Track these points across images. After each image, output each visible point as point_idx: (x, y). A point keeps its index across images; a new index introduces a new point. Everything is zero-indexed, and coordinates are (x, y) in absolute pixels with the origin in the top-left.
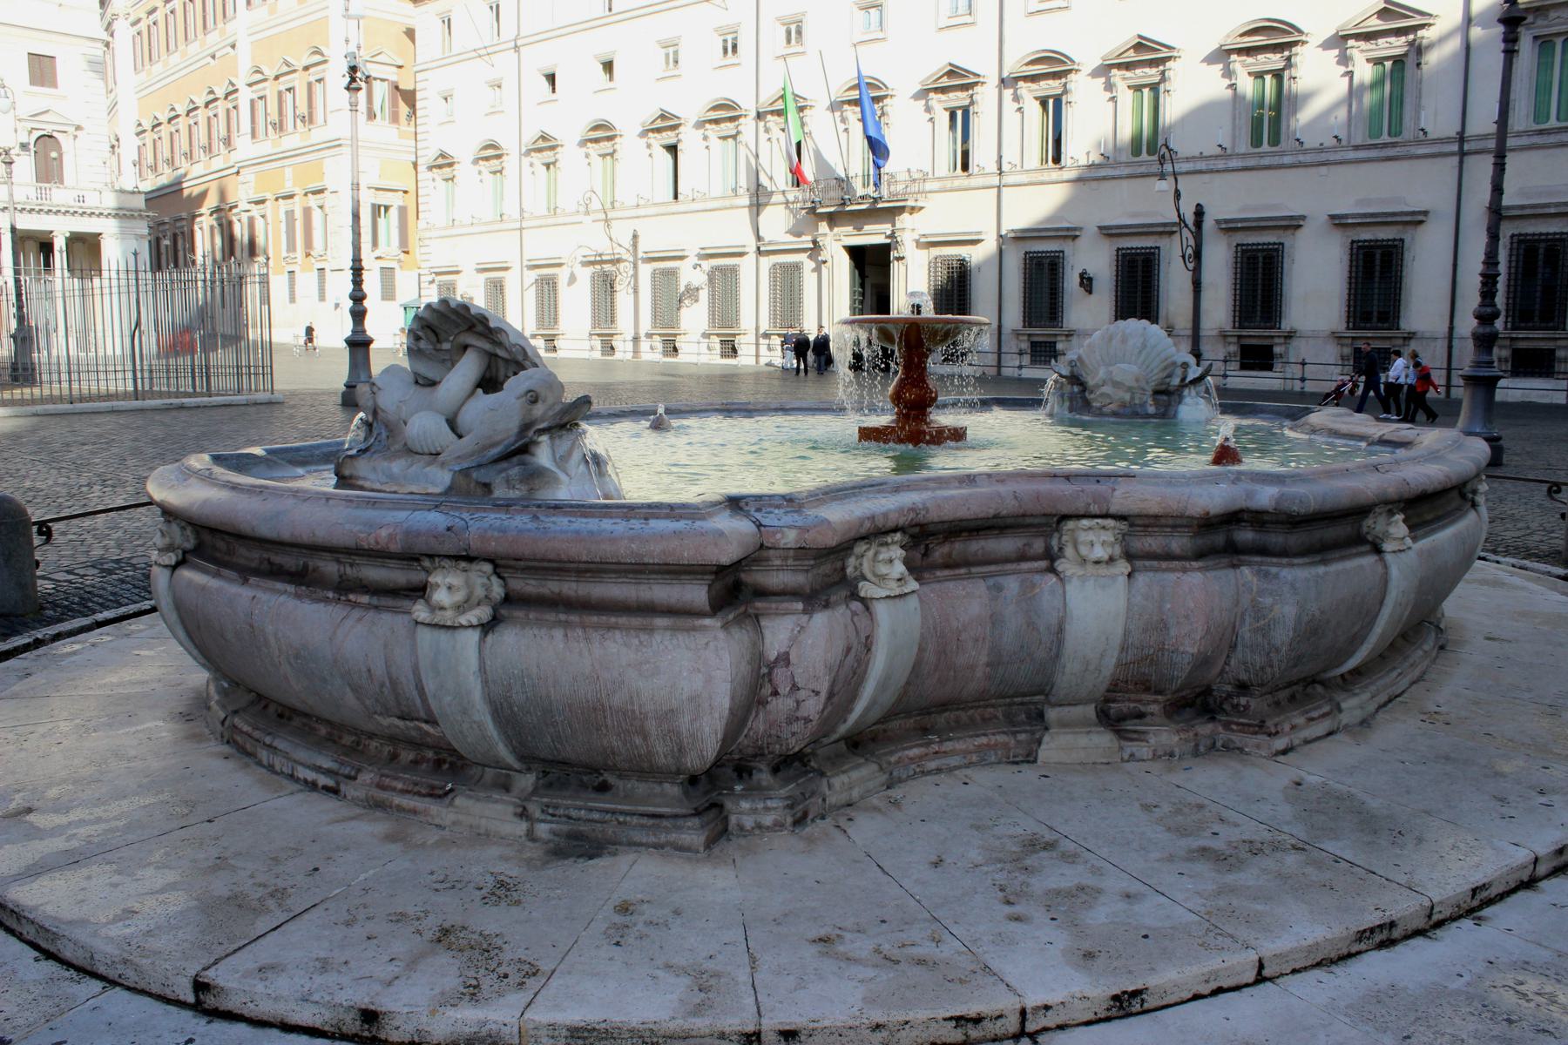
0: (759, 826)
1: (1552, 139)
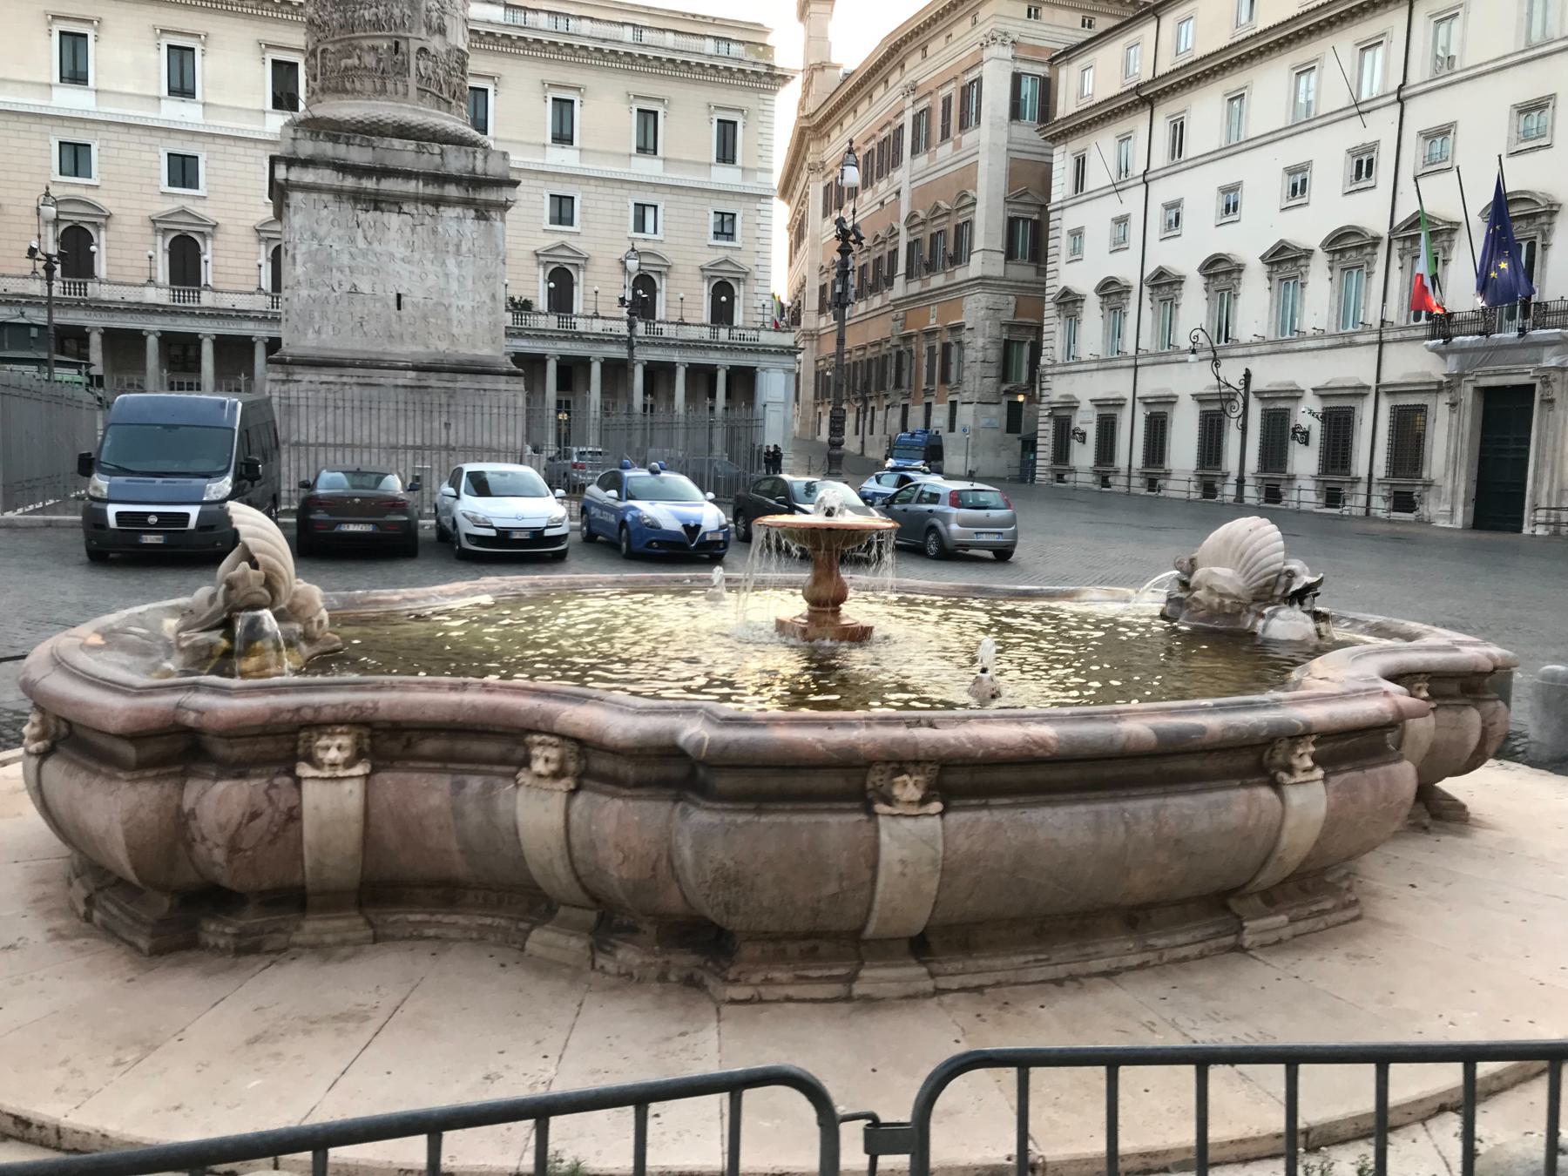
0: (216, 946)
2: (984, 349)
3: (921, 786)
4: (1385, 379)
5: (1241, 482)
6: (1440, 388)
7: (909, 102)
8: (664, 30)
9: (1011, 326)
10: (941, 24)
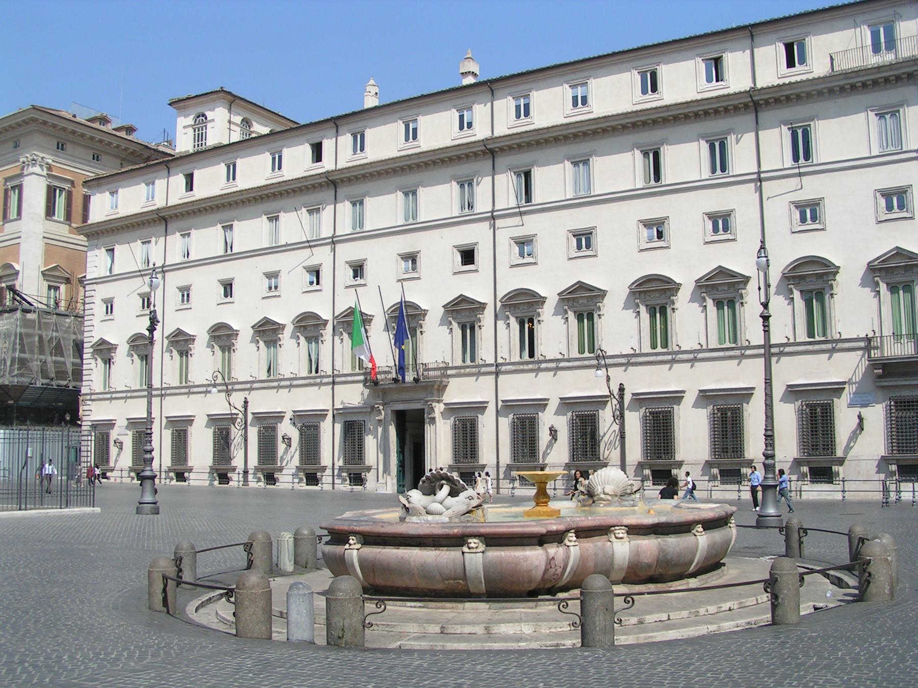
1: (817, 347)
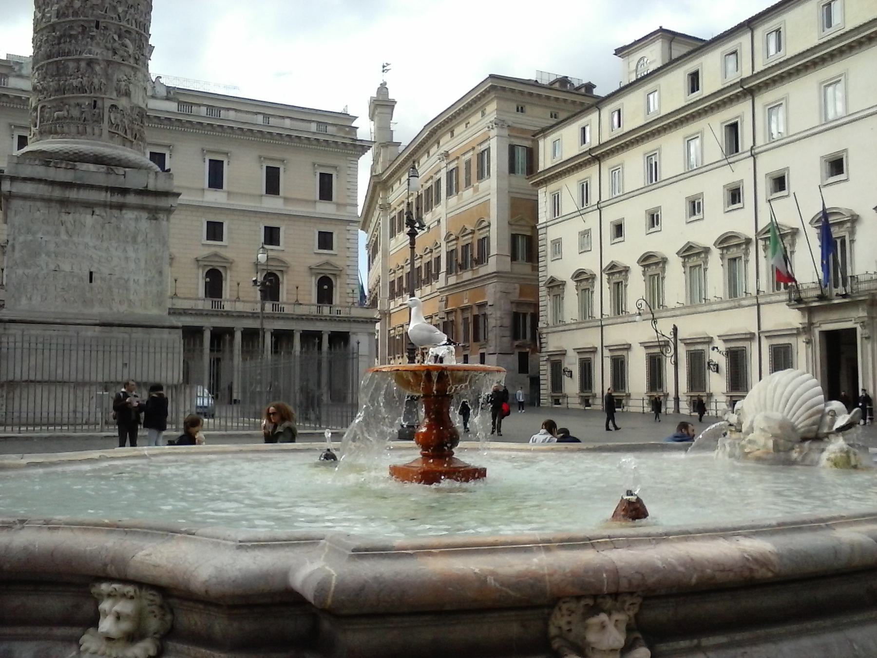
2: (501, 318)
3: (623, 627)
4: (763, 328)
5: (677, 399)
6: (798, 333)
7: (443, 164)
8: (283, 117)
9: (519, 304)
10: (463, 116)
